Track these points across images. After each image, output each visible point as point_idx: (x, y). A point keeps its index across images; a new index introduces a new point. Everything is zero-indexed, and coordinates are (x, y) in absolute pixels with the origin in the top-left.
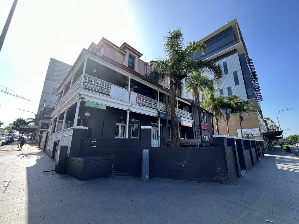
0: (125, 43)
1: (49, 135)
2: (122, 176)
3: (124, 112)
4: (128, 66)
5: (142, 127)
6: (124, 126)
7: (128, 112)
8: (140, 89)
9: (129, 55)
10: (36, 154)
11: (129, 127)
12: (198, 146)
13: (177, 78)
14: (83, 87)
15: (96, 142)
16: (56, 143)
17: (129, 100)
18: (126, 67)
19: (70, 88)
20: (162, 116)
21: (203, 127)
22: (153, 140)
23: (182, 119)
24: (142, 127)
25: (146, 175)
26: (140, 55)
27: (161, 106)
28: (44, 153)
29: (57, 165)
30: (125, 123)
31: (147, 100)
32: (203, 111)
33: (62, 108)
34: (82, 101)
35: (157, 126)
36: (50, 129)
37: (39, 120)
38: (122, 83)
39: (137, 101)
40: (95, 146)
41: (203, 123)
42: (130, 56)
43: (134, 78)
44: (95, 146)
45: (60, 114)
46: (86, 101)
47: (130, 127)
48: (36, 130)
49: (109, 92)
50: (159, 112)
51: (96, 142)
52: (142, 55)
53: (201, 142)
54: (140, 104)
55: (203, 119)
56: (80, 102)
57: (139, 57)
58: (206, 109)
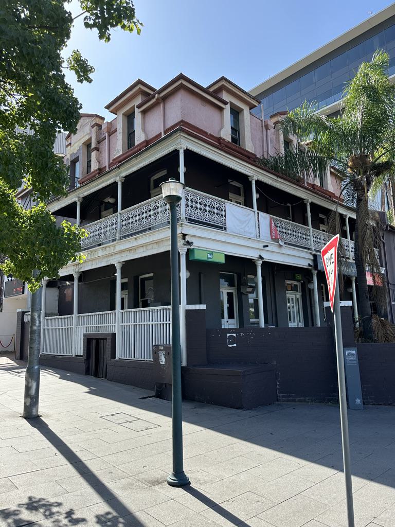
2: (298, 403)
3: (246, 265)
4: (230, 141)
8: (273, 202)
15: (235, 335)
18: (229, 142)
25: (356, 399)
39: (274, 235)
40: (235, 345)
43: (262, 178)
44: (235, 345)
51: (235, 335)
54: (280, 242)
56: (185, 253)
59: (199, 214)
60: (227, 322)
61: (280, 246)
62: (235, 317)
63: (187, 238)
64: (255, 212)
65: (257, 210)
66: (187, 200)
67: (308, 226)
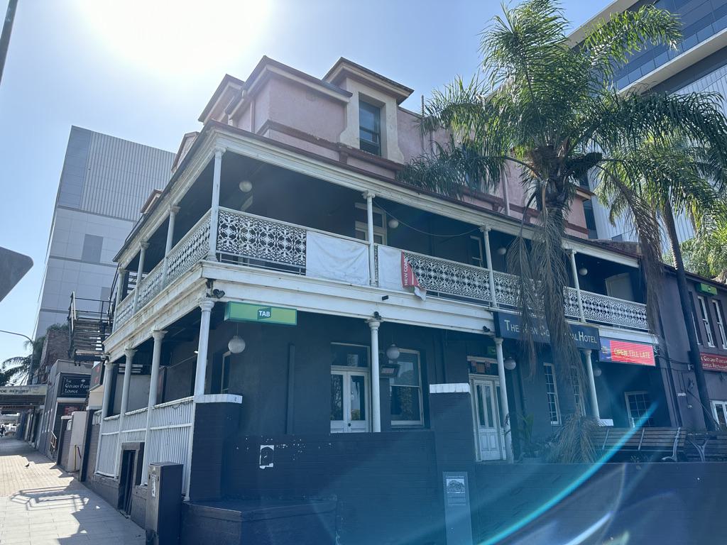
0: (342, 61)
1: (99, 419)
3: (357, 327)
5: (435, 389)
6: (362, 378)
7: (375, 325)
8: (416, 233)
9: (360, 101)
10: (62, 494)
11: (380, 379)
12: (674, 457)
13: (559, 174)
14: (218, 255)
15: (272, 447)
16: (133, 453)
17: (374, 281)
18: (354, 149)
19: (167, 254)
20: (510, 328)
21: (707, 363)
22: (481, 430)
23: (603, 332)
24: (435, 389)
26: (400, 93)
27: (497, 286)
28: (86, 490)
29: (152, 531)
30: (365, 362)
31: (441, 272)
32: (705, 287)
33: (142, 321)
34: (217, 304)
35: (494, 370)
36: (98, 397)
37: (50, 360)
38: (339, 212)
39: (406, 280)
40: (271, 465)
41: (711, 345)
42: (365, 103)
43: (385, 194)
44: (271, 465)
45: (133, 347)
46: (229, 302)
47: (384, 379)
48: (38, 399)
49: (302, 259)
50: (496, 314)
51: (272, 447)
52: (411, 91)
53: (687, 438)
55: (708, 327)
56: (210, 309)
57: (399, 103)
58: (718, 279)
59: (445, 286)
60: (349, 425)
61: (419, 298)
62: (421, 418)
63: (216, 286)
64: (369, 246)
65: (494, 269)
66: (497, 284)
67: (487, 268)
